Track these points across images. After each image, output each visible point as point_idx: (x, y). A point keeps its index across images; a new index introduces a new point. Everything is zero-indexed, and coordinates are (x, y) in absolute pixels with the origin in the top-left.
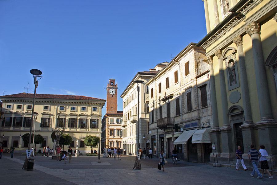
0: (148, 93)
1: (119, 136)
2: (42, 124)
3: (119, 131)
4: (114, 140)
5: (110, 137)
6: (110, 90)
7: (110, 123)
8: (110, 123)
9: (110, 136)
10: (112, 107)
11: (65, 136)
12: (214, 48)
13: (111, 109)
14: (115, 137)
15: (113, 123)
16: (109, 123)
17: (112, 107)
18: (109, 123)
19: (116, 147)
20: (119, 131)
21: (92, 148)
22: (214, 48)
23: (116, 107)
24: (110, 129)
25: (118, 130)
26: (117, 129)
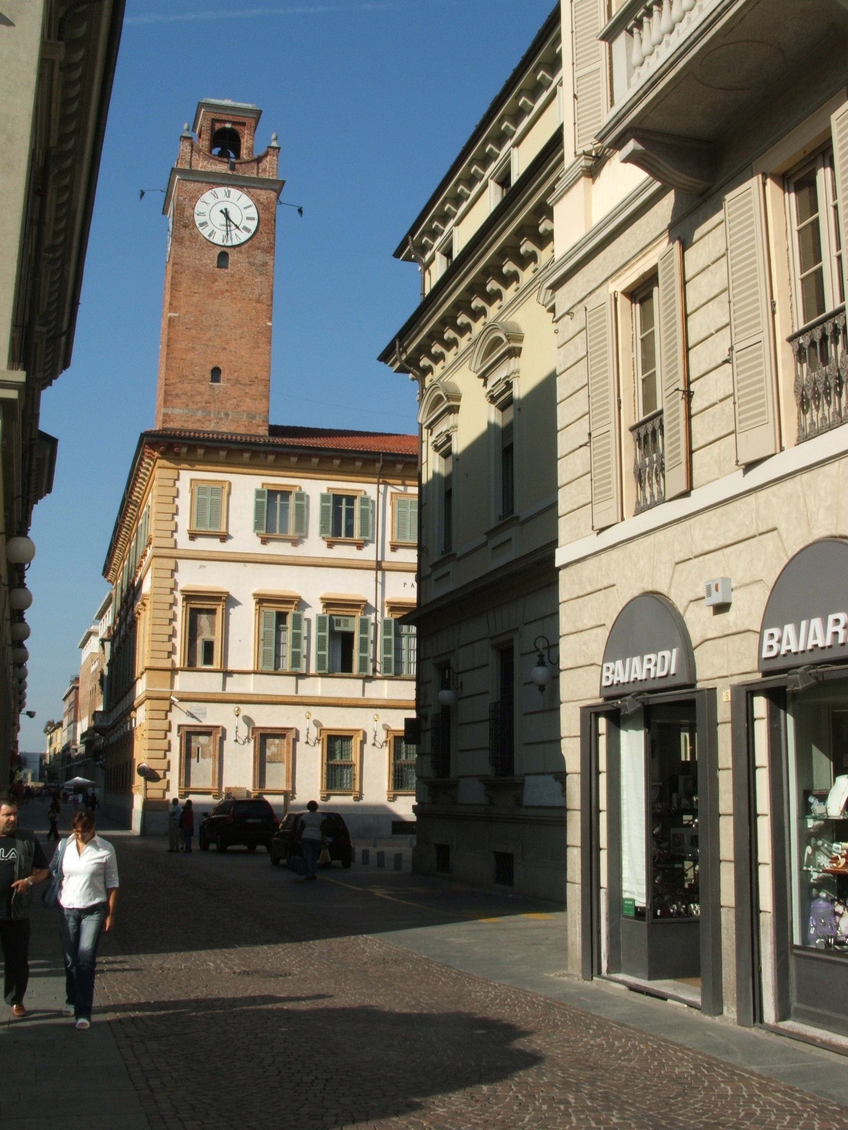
0: (34, 713)
1: (277, 671)
2: (784, 1091)
3: (281, 617)
4: (212, 716)
5: (185, 682)
6: (208, 196)
7: (193, 536)
8: (193, 536)
9: (191, 666)
10: (216, 373)
11: (8, 827)
12: (709, 232)
13: (205, 387)
14: (236, 686)
15: (224, 538)
16: (182, 538)
17: (216, 373)
18: (182, 538)
19: (351, 798)
20: (281, 617)
21: (102, 971)
22: (709, 232)
23: (262, 375)
24: (189, 597)
25: (272, 610)
26: (262, 600)
